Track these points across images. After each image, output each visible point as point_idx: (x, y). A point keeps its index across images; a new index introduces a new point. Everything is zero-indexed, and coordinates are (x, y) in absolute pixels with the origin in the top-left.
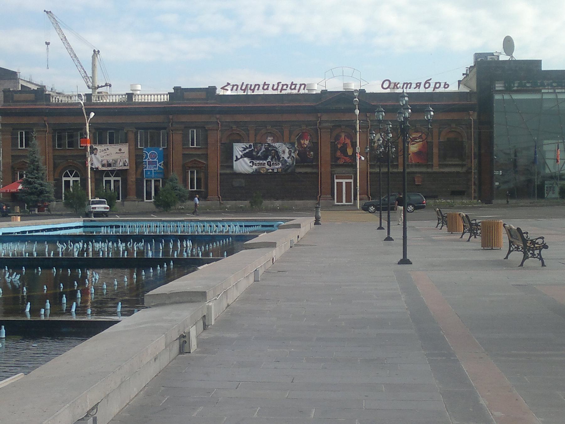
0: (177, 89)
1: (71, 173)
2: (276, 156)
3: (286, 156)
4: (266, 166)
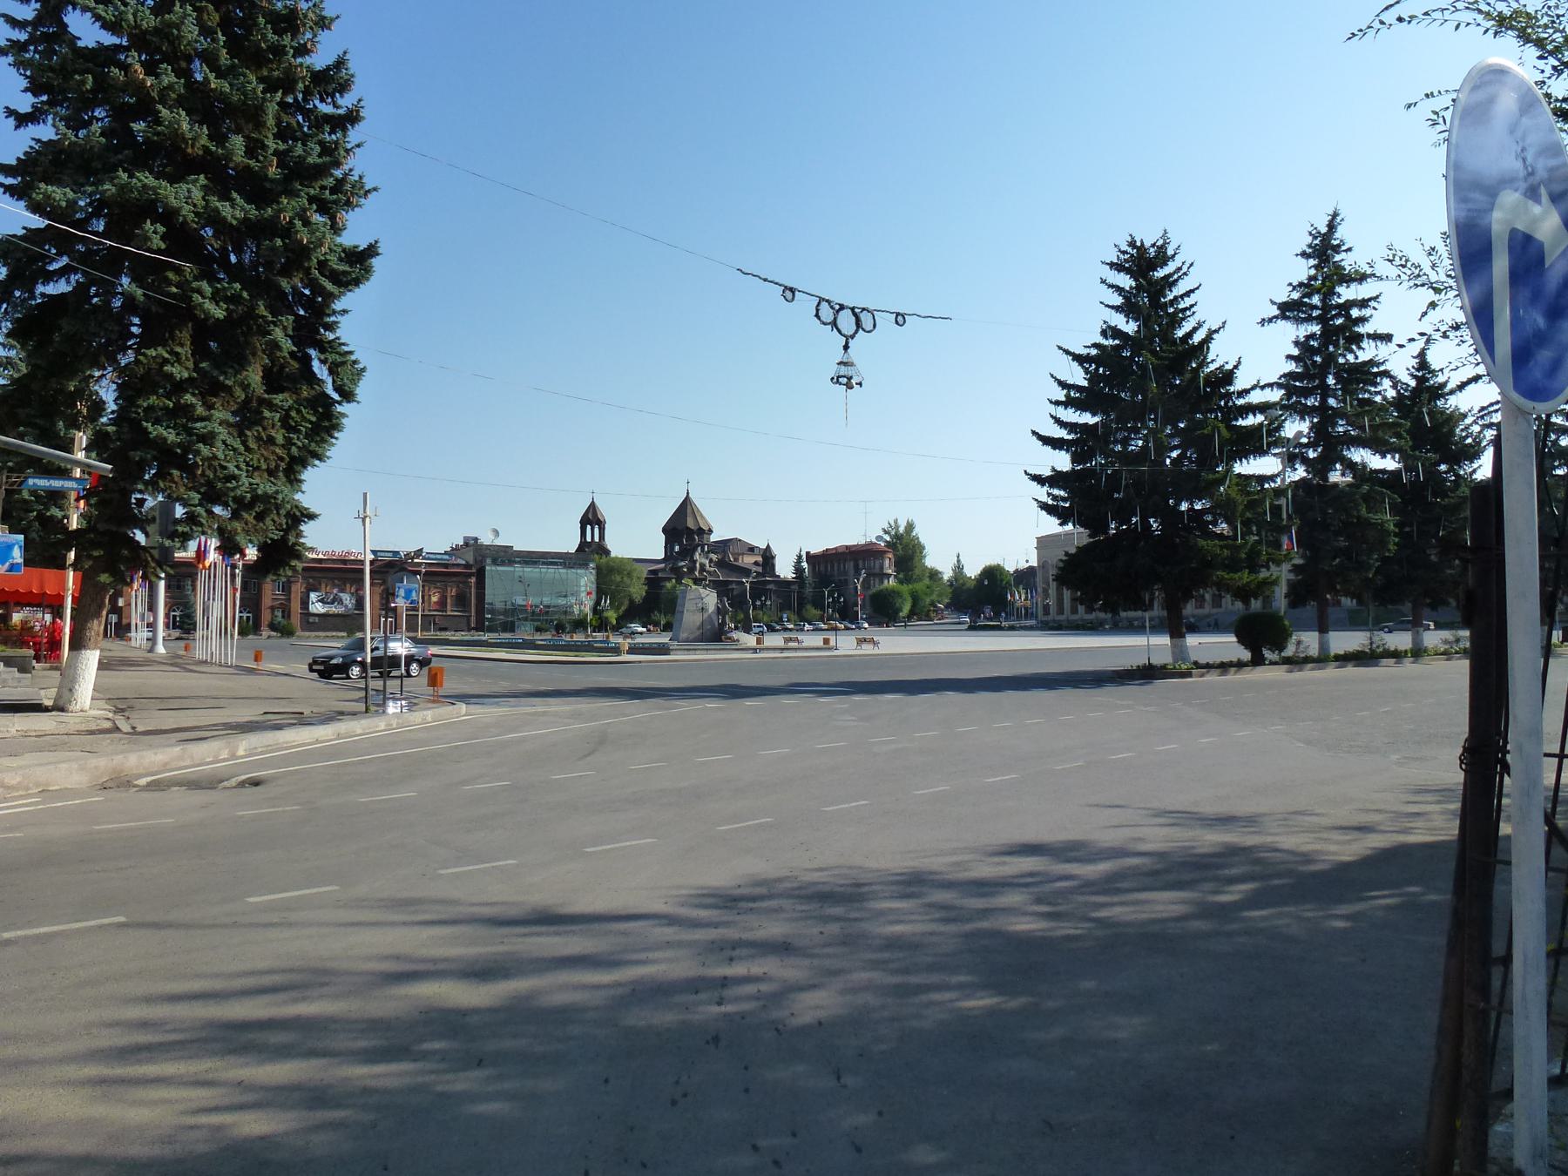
0: (337, 427)
1: (245, 610)
2: (341, 602)
3: (348, 602)
4: (334, 609)
